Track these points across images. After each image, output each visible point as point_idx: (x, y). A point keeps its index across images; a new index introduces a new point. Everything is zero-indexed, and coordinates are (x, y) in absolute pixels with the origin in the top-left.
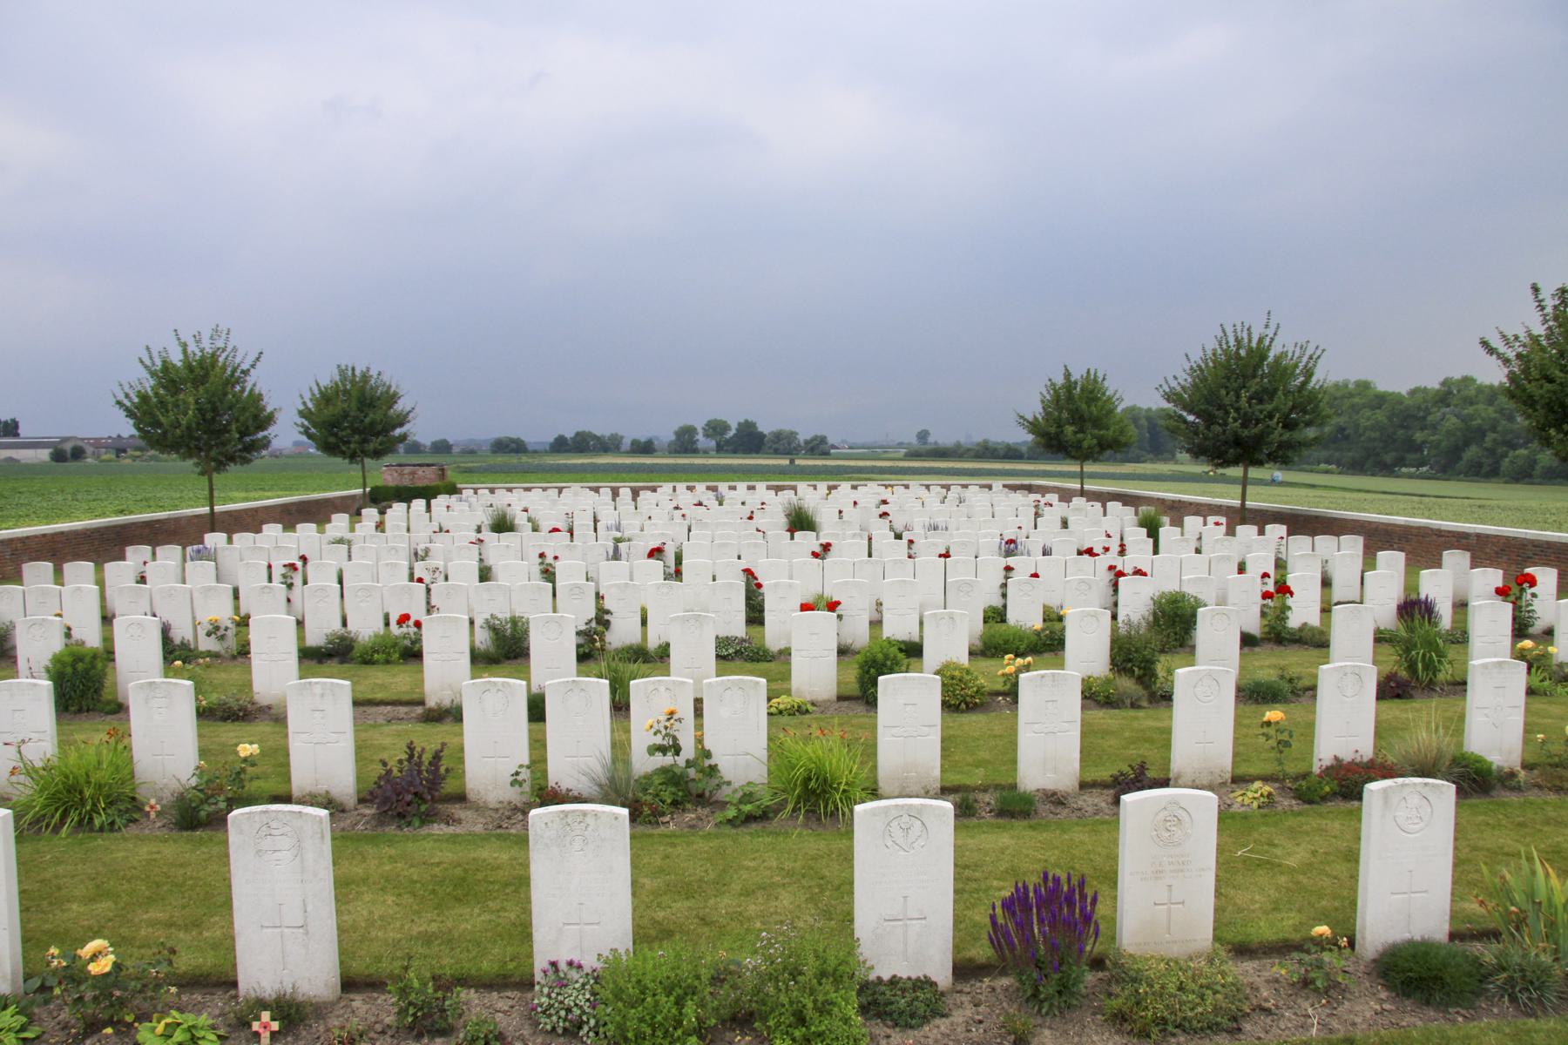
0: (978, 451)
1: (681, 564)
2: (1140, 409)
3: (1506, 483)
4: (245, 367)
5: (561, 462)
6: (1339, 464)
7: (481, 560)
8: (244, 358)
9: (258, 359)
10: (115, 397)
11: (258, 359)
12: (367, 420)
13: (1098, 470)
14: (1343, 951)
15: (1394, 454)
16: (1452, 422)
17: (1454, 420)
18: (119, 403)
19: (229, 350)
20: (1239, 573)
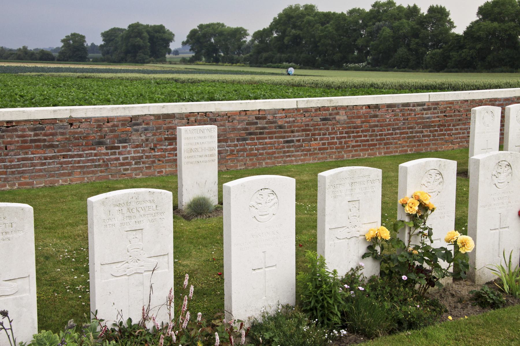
0: (20, 55)
1: (500, 139)
3: (430, 72)
5: (117, 68)
6: (296, 63)
13: (123, 68)
15: (462, 56)
16: (387, 31)
17: (388, 30)
20: (500, 150)
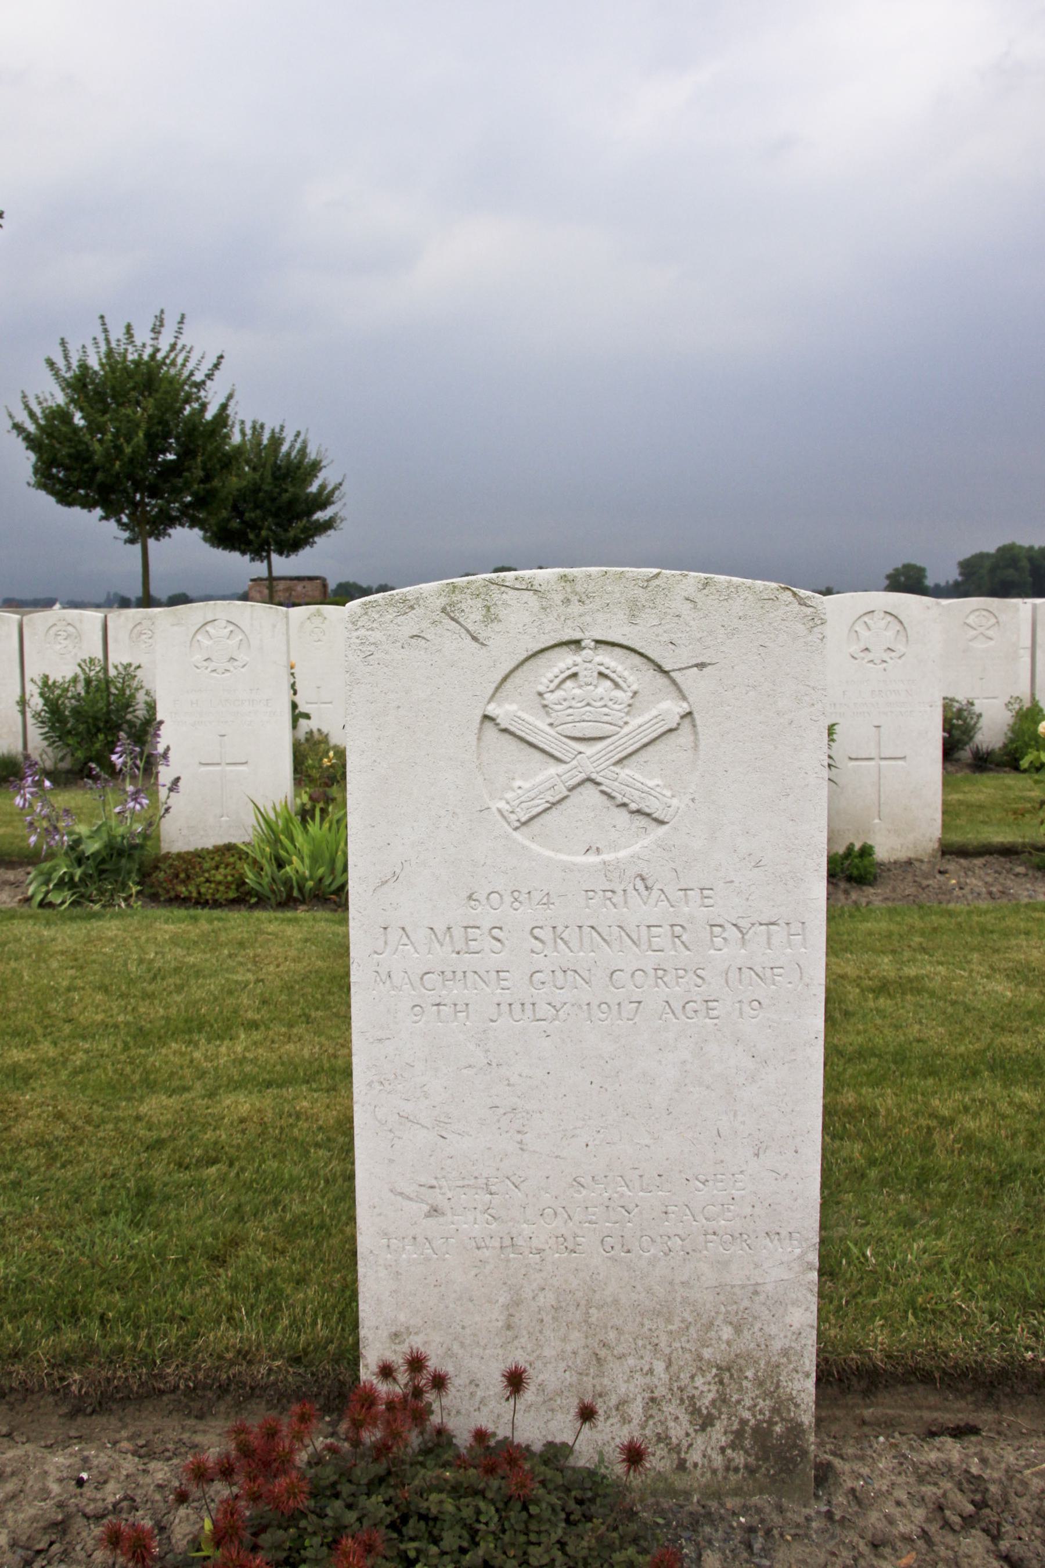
2: (1021, 547)
4: (198, 377)
7: (297, 716)
8: (199, 364)
9: (216, 366)
10: (11, 416)
11: (216, 366)
12: (286, 496)
14: (459, 1014)
18: (18, 427)
19: (179, 347)
